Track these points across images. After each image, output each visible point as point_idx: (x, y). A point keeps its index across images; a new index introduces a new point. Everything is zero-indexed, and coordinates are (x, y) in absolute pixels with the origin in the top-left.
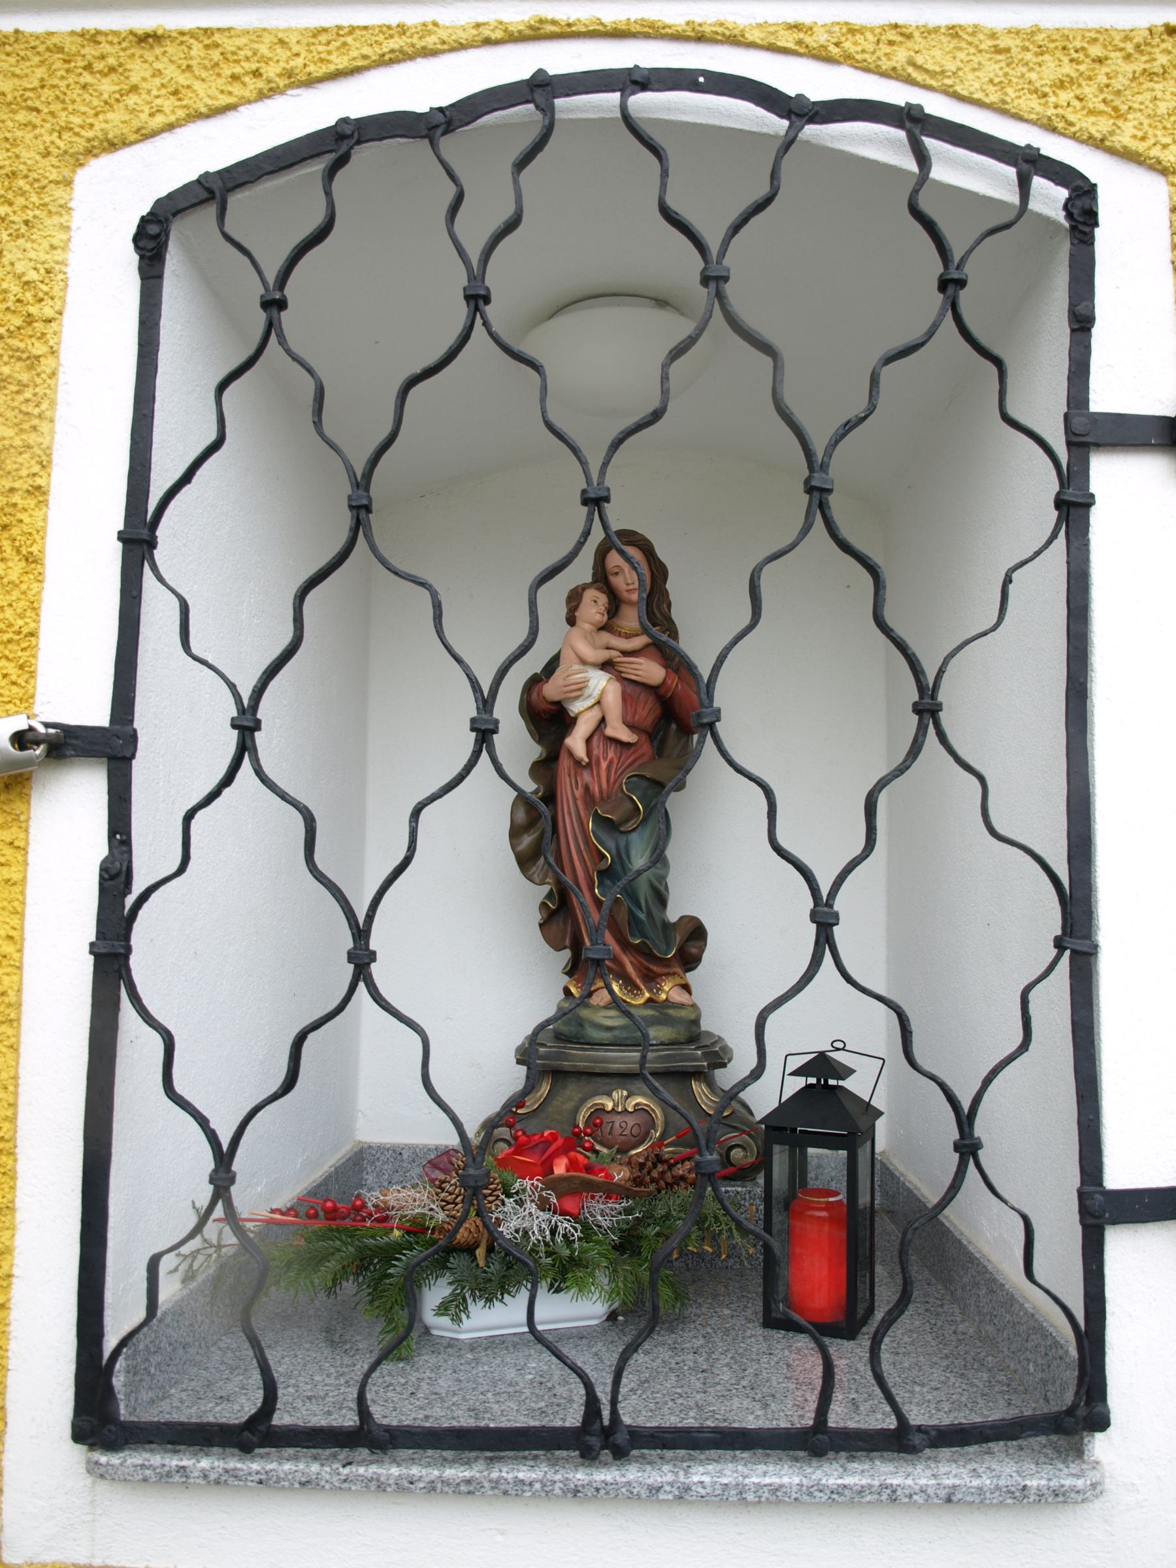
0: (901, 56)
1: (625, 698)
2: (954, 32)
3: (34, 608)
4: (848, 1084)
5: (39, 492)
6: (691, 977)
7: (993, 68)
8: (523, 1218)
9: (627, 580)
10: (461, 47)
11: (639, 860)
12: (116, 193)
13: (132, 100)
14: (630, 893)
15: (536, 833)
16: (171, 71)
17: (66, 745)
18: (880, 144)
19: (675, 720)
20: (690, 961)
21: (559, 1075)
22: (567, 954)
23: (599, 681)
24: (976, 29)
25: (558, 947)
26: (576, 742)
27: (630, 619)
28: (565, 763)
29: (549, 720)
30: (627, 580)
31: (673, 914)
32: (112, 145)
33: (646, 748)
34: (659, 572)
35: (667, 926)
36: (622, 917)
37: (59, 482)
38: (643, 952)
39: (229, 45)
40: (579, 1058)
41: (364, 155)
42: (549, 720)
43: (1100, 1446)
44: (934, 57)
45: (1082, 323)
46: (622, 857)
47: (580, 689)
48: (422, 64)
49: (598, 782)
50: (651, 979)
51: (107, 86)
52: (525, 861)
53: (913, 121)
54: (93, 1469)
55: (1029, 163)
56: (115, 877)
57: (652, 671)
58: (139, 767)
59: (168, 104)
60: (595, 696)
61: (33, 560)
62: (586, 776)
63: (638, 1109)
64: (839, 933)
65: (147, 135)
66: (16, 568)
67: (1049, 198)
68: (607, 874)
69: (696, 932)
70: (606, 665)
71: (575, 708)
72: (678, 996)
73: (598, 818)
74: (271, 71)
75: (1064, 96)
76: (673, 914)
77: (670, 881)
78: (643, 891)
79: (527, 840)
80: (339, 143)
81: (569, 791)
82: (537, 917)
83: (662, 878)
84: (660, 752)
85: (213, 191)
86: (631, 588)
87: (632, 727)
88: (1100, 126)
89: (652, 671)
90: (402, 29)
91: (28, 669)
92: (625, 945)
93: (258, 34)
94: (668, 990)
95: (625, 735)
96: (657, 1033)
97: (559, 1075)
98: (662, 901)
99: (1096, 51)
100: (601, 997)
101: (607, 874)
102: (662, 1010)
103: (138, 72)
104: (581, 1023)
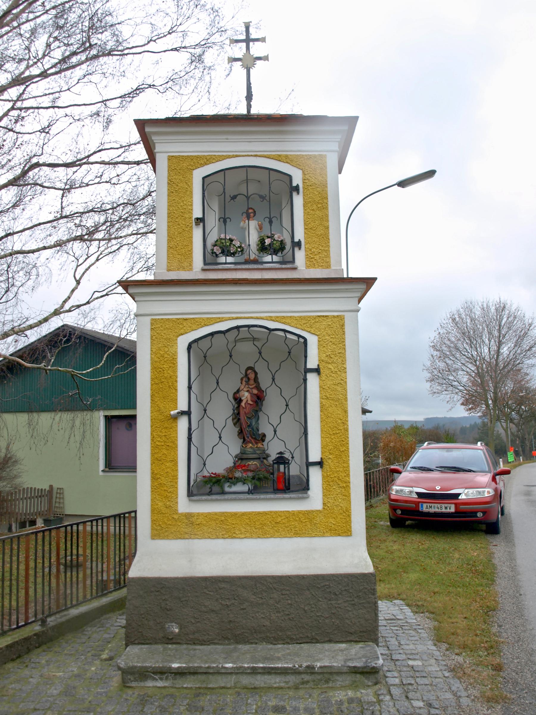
0: (284, 320)
1: (251, 396)
2: (291, 317)
3: (177, 396)
4: (284, 455)
5: (176, 381)
6: (263, 443)
7: (296, 322)
8: (238, 474)
9: (252, 376)
10: (227, 320)
11: (254, 423)
12: (183, 342)
13: (185, 328)
14: (253, 429)
15: (237, 418)
16: (189, 324)
17: (183, 413)
18: (282, 334)
19: (259, 398)
20: (263, 440)
21: (242, 459)
22: (242, 440)
23: (247, 394)
24: (293, 317)
25: (241, 439)
26: (243, 404)
27: (252, 382)
28: (241, 408)
29: (238, 400)
30: (252, 376)
31: (260, 432)
32: (182, 334)
33: (255, 405)
34: (256, 374)
35: (259, 435)
36: (252, 433)
37: (179, 379)
38: (255, 439)
39: (197, 320)
40: (245, 456)
41: (215, 335)
42: (238, 400)
43: (309, 492)
44: (288, 321)
45: (306, 357)
46: (251, 424)
47: (243, 396)
48: (222, 323)
49: (247, 411)
50: (257, 443)
51: (181, 326)
52: (235, 424)
53: (285, 331)
54: (190, 500)
55: (299, 336)
56: (190, 429)
57: (255, 392)
58: (192, 415)
59: (189, 329)
60: (246, 396)
61: (176, 390)
62: (245, 410)
63: (255, 464)
64: (277, 433)
65: (186, 333)
66: (174, 391)
67: (302, 340)
68: (249, 426)
69: (264, 435)
70: (248, 391)
71: (243, 398)
72: (261, 446)
73: (247, 417)
74: (202, 324)
75: (305, 325)
76: (260, 432)
77: (260, 427)
78: (255, 429)
79: (235, 421)
80: (212, 334)
81: (242, 412)
82: (237, 434)
83: (258, 427)
84: (257, 405)
85: (196, 341)
86: (250, 376)
87: (252, 401)
88: (309, 330)
89: (255, 392)
90: (219, 318)
91: (176, 403)
92: (252, 437)
93: (200, 318)
94: (259, 445)
95: (251, 403)
96: (258, 452)
97: (242, 459)
98: (258, 431)
99: (309, 319)
100: (248, 447)
101: (249, 426)
102: (259, 448)
103: (185, 324)
104: (245, 451)
